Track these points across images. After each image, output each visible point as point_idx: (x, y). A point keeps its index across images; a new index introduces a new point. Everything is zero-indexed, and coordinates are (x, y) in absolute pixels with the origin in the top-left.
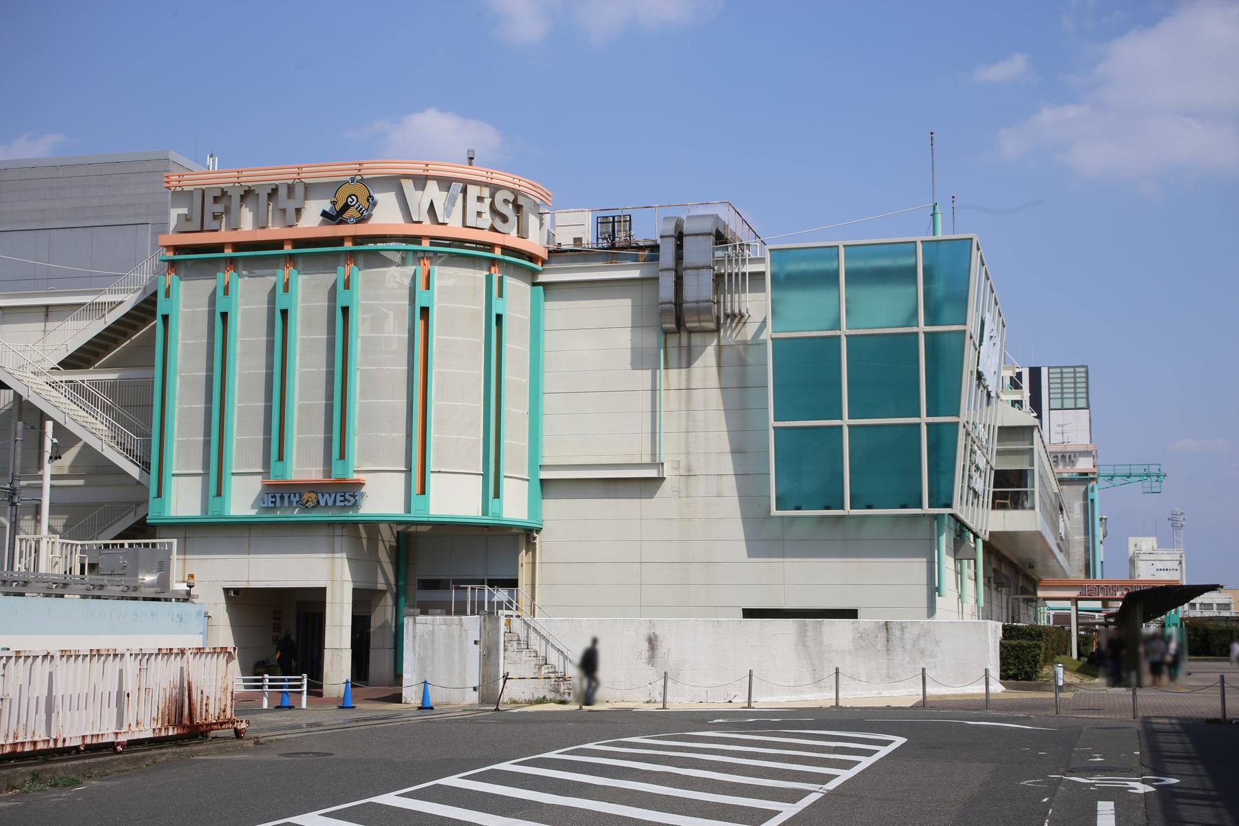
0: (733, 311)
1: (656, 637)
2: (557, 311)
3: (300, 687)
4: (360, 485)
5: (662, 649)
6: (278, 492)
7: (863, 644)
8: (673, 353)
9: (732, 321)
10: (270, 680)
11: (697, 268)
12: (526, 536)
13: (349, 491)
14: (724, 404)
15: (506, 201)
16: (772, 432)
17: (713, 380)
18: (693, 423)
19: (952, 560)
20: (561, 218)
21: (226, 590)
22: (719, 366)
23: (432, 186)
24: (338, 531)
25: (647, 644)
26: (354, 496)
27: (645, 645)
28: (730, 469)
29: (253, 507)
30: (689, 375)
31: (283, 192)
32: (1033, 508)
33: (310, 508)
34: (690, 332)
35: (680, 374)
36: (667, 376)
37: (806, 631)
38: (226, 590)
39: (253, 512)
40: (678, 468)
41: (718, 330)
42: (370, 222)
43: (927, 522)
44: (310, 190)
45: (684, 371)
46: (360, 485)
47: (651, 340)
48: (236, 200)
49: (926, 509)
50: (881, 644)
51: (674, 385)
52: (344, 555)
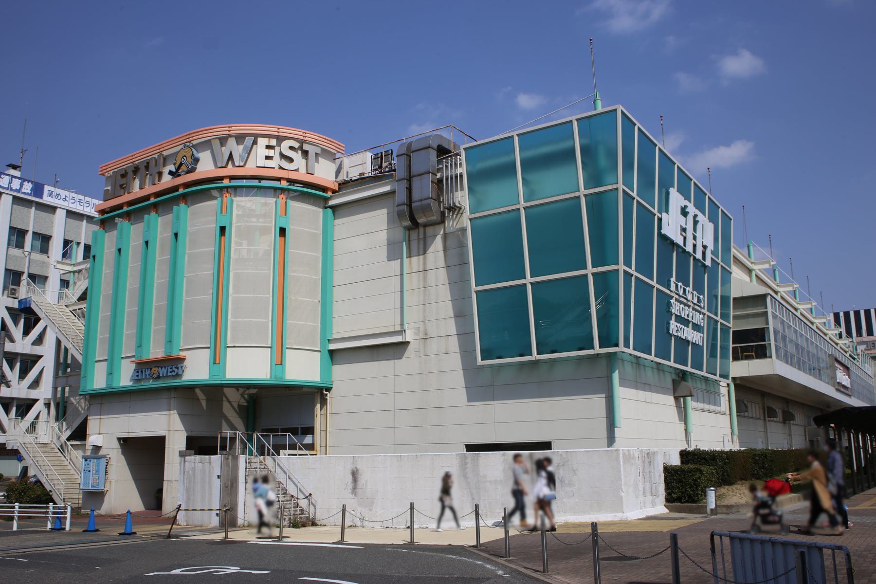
0: (454, 204)
1: (357, 470)
2: (344, 225)
3: (47, 513)
4: (182, 360)
5: (361, 482)
6: (144, 367)
8: (414, 244)
10: (13, 512)
11: (421, 175)
12: (318, 394)
13: (174, 363)
14: (449, 279)
15: (291, 148)
17: (441, 262)
18: (414, 297)
20: (347, 162)
21: (119, 439)
22: (445, 250)
23: (232, 142)
25: (351, 477)
26: (177, 368)
27: (350, 478)
28: (454, 331)
30: (425, 259)
32: (771, 357)
33: (159, 380)
34: (425, 226)
35: (419, 260)
36: (410, 263)
37: (466, 464)
38: (119, 439)
39: (131, 384)
40: (418, 333)
42: (197, 171)
43: (604, 362)
44: (165, 160)
45: (421, 257)
46: (182, 360)
47: (400, 233)
48: (130, 174)
49: (597, 349)
51: (415, 269)
52: (175, 412)
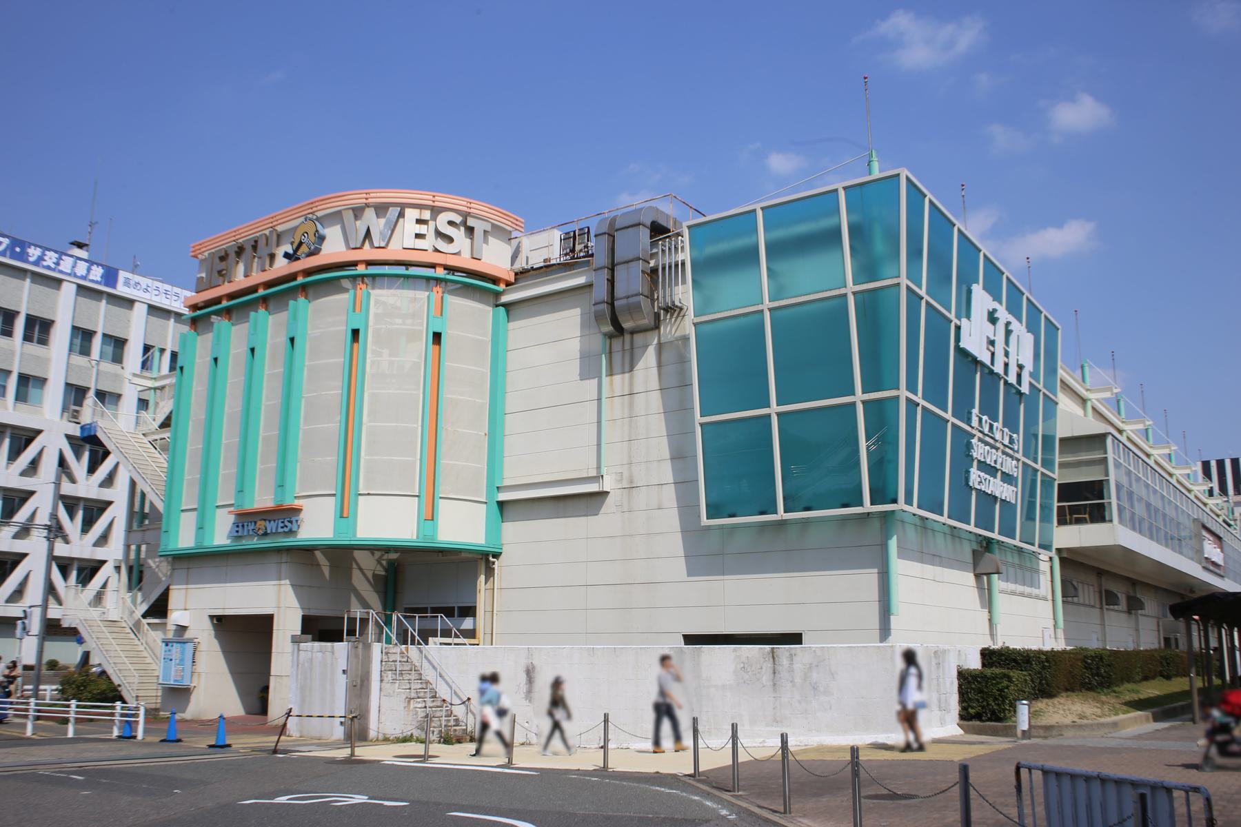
0: (673, 302)
1: (534, 667)
2: (523, 329)
3: (113, 715)
4: (297, 511)
7: (746, 677)
8: (617, 358)
9: (672, 316)
11: (627, 262)
13: (286, 515)
14: (664, 406)
15: (451, 223)
16: (698, 429)
17: (654, 383)
19: (970, 578)
21: (212, 617)
22: (660, 366)
23: (370, 214)
24: (284, 558)
27: (523, 677)
28: (669, 477)
29: (229, 537)
30: (631, 378)
31: (262, 243)
32: (1111, 521)
33: (265, 538)
35: (623, 379)
36: (611, 384)
38: (212, 617)
39: (228, 542)
41: (657, 327)
43: (876, 524)
45: (627, 375)
46: (297, 511)
48: (232, 255)
49: (868, 507)
50: (766, 678)
